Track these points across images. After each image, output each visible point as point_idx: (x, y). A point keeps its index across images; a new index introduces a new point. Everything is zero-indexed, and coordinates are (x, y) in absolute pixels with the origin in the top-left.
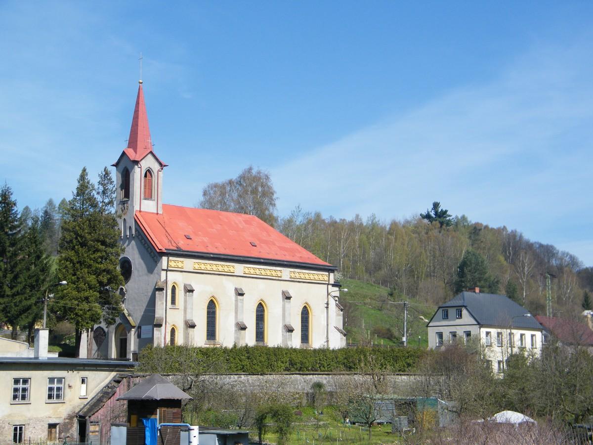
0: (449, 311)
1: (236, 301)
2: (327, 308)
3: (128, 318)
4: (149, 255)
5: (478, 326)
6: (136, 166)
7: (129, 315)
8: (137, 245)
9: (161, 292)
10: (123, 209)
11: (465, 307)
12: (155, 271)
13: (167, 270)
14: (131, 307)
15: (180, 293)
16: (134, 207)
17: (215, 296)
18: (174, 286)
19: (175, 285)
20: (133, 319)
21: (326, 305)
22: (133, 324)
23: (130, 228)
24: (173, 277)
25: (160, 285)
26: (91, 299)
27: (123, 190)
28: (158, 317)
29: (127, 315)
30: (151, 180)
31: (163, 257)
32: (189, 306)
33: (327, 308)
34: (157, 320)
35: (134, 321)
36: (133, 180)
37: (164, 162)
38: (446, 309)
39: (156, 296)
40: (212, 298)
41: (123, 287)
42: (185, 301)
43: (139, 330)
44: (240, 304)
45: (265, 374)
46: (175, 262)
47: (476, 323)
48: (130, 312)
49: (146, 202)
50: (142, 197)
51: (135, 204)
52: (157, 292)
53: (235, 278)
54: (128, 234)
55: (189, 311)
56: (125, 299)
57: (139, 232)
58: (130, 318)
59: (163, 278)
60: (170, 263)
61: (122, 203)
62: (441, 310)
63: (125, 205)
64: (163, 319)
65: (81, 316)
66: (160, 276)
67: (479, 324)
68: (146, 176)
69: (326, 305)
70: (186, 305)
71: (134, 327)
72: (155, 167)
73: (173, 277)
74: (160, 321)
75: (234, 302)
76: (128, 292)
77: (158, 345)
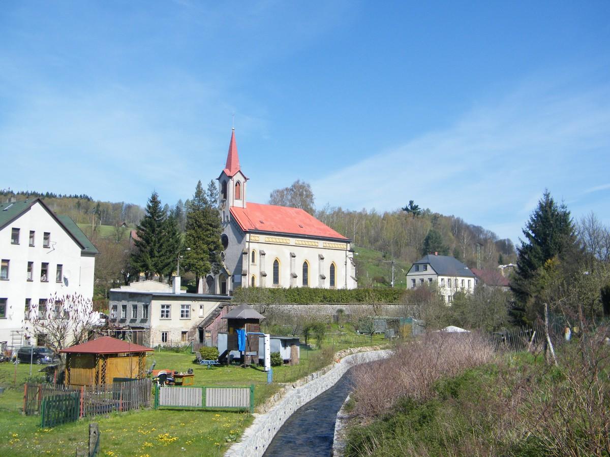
1: (291, 260)
2: (346, 264)
11: (429, 264)
13: (249, 242)
15: (257, 256)
24: (253, 246)
25: (245, 251)
37: (247, 177)
42: (260, 261)
46: (254, 237)
55: (262, 266)
58: (227, 271)
65: (199, 269)
67: (437, 274)
68: (236, 185)
71: (230, 276)
73: (253, 246)
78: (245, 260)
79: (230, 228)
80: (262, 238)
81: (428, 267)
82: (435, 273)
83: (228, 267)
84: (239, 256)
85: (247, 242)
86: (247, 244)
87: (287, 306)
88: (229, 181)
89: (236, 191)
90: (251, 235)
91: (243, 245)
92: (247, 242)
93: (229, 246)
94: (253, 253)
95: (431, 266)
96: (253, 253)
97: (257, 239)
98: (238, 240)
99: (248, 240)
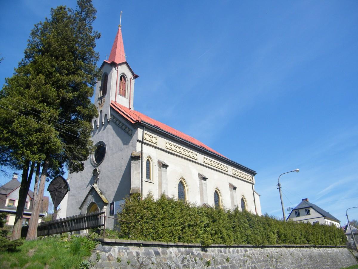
0: (300, 211)
1: (201, 184)
2: (279, 188)
3: (100, 195)
4: (123, 132)
5: (323, 218)
6: (114, 68)
7: (101, 193)
8: (114, 129)
9: (137, 161)
10: (100, 103)
11: (312, 207)
12: (130, 144)
13: (142, 142)
14: (103, 186)
15: (154, 168)
16: (110, 97)
17: (184, 177)
18: (148, 160)
19: (149, 159)
20: (105, 197)
21: (278, 187)
22: (105, 201)
23: (106, 115)
24: (147, 151)
25: (136, 154)
26: (42, 115)
27: (102, 91)
28: (134, 188)
29: (99, 193)
30: (125, 84)
31: (138, 128)
32: (164, 181)
33: (279, 188)
34: (133, 190)
35: (107, 199)
36: (111, 78)
37: (136, 73)
38: (298, 210)
39: (132, 165)
40: (181, 179)
41: (97, 169)
42: (160, 176)
43: (112, 206)
44: (204, 187)
45: (266, 247)
46: (149, 137)
47: (321, 216)
48: (102, 190)
49: (121, 97)
50: (118, 92)
51: (111, 96)
52: (133, 162)
53: (198, 165)
54: (104, 121)
55: (164, 186)
56: (98, 179)
57: (113, 116)
58: (102, 196)
59: (138, 149)
60: (145, 136)
61: (100, 99)
62: (294, 212)
63: (103, 99)
64: (139, 189)
65: (21, 136)
66: (135, 147)
67: (324, 216)
68: (121, 79)
69: (278, 187)
70: (161, 180)
71: (106, 204)
72: (129, 75)
73: (147, 151)
74: (137, 190)
75: (199, 186)
76: (101, 172)
77: (149, 194)
78: (136, 170)
79: (113, 132)
80: (162, 142)
81: (311, 210)
82: (321, 216)
83: (104, 191)
84: (124, 168)
85: (139, 141)
86: (139, 145)
87: (246, 251)
88: (111, 70)
89: (120, 88)
90: (145, 132)
91: (131, 148)
92: (139, 141)
93: (106, 156)
94: (148, 162)
95: (291, 213)
96: (148, 162)
97: (154, 140)
98: (122, 140)
99: (140, 138)
